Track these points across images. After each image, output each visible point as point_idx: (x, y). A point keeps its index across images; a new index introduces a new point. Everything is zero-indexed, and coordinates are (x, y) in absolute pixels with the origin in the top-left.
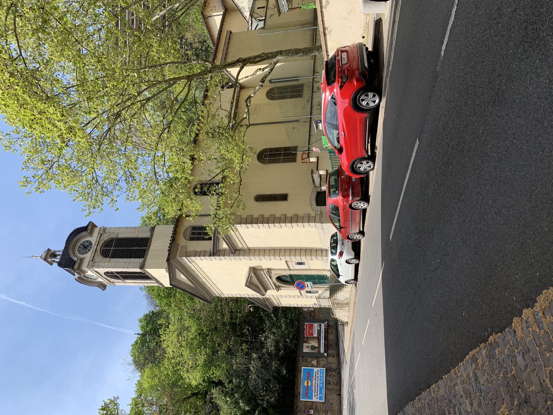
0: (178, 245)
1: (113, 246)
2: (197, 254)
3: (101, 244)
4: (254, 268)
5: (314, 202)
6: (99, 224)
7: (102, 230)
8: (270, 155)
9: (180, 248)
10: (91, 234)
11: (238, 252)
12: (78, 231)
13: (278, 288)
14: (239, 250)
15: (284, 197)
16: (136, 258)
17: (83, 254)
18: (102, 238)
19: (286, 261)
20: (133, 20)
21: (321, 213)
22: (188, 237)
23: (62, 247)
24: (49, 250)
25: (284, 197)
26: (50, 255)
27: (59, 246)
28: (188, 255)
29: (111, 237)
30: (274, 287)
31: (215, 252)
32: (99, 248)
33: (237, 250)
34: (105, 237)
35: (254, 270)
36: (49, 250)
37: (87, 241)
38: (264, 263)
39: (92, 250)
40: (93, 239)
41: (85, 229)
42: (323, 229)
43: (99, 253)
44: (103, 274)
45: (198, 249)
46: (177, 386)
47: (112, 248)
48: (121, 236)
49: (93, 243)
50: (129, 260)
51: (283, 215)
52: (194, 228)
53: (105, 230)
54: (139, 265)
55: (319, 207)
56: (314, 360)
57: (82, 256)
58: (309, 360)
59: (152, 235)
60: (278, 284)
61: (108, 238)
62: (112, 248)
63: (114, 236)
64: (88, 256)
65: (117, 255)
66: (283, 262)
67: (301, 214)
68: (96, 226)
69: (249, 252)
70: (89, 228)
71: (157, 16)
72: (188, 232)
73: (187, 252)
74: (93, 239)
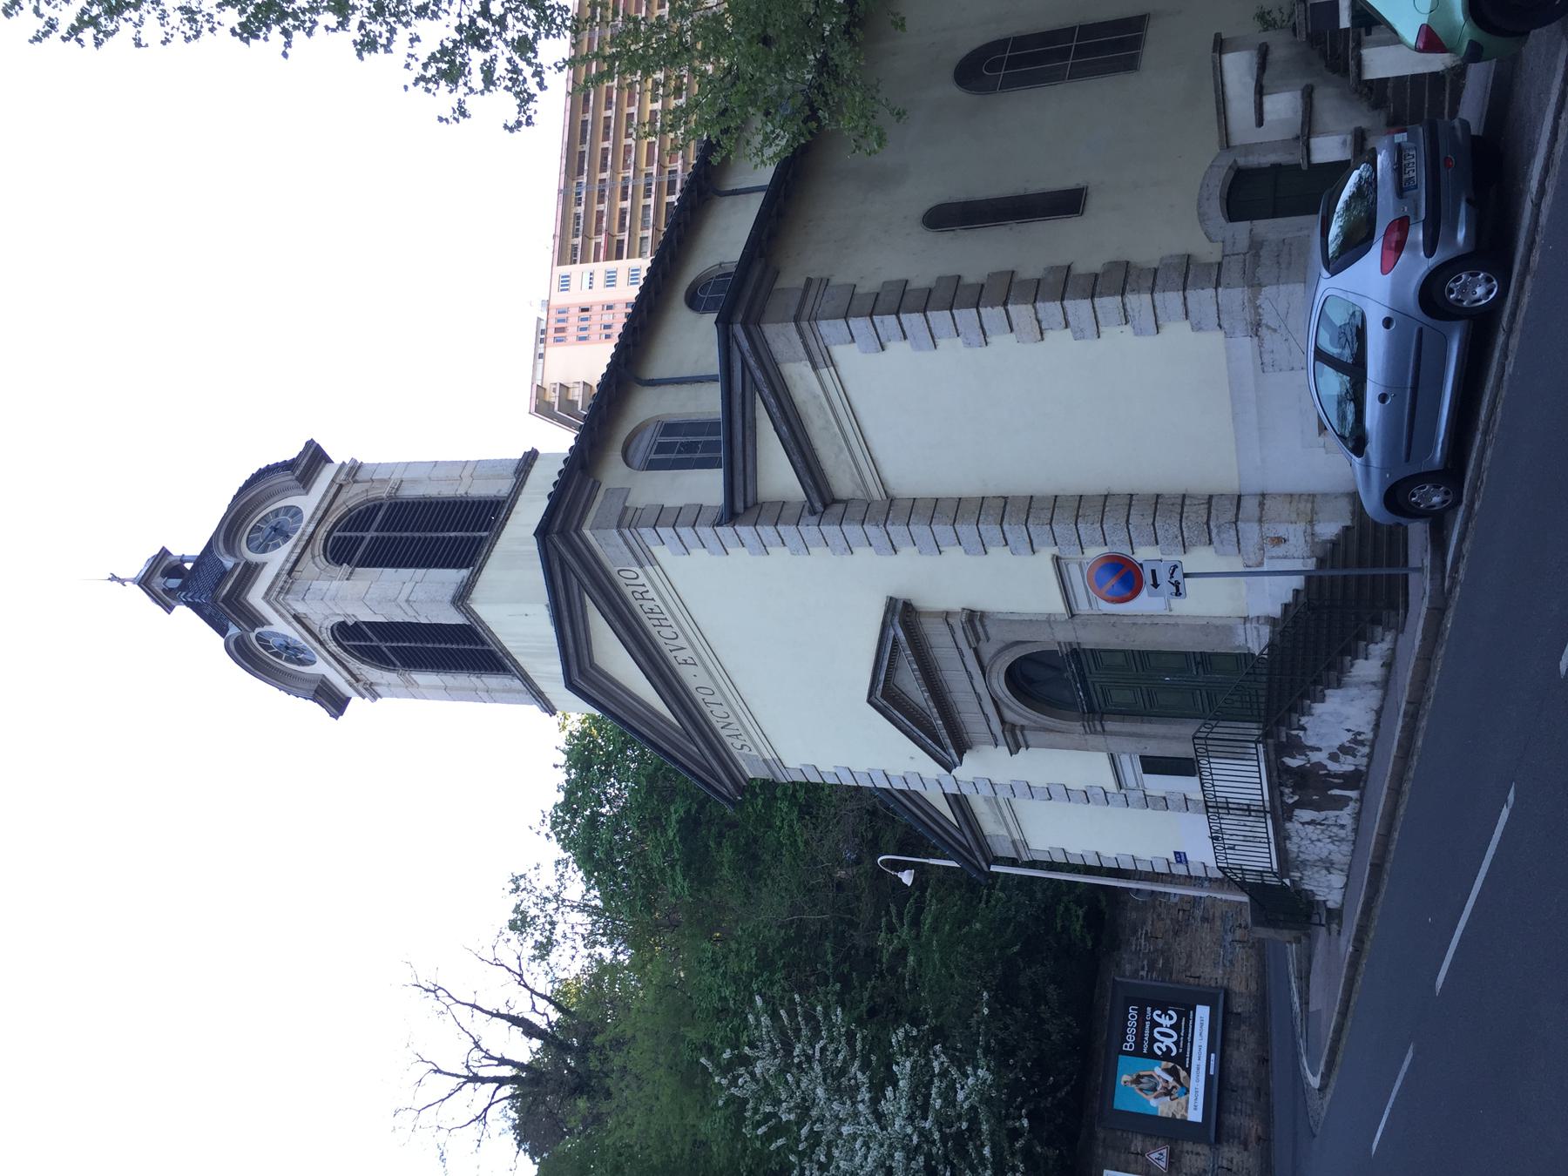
0: (597, 485)
1: (375, 525)
2: (664, 517)
3: (332, 519)
4: (908, 607)
5: (1215, 208)
6: (339, 453)
7: (346, 470)
8: (1013, 62)
9: (599, 498)
11: (839, 508)
13: (1015, 740)
14: (846, 502)
15: (1069, 203)
16: (448, 567)
17: (264, 551)
19: (1057, 560)
21: (1256, 246)
22: (638, 458)
24: (164, 553)
25: (1069, 203)
28: (627, 520)
29: (373, 494)
30: (996, 726)
31: (741, 507)
33: (835, 501)
34: (353, 496)
35: (902, 616)
36: (164, 553)
37: (288, 509)
38: (951, 578)
39: (295, 537)
40: (308, 503)
42: (1256, 328)
45: (673, 501)
47: (369, 535)
48: (410, 492)
49: (307, 514)
50: (420, 572)
51: (1052, 270)
52: (670, 428)
53: (353, 471)
54: (450, 591)
55: (1243, 227)
56: (1155, 1147)
57: (254, 557)
58: (1137, 1144)
60: (1018, 713)
62: (369, 535)
63: (383, 492)
64: (276, 559)
65: (385, 555)
66: (1043, 562)
67: (1146, 254)
68: (329, 461)
69: (888, 512)
72: (644, 444)
73: (626, 509)
74: (308, 503)
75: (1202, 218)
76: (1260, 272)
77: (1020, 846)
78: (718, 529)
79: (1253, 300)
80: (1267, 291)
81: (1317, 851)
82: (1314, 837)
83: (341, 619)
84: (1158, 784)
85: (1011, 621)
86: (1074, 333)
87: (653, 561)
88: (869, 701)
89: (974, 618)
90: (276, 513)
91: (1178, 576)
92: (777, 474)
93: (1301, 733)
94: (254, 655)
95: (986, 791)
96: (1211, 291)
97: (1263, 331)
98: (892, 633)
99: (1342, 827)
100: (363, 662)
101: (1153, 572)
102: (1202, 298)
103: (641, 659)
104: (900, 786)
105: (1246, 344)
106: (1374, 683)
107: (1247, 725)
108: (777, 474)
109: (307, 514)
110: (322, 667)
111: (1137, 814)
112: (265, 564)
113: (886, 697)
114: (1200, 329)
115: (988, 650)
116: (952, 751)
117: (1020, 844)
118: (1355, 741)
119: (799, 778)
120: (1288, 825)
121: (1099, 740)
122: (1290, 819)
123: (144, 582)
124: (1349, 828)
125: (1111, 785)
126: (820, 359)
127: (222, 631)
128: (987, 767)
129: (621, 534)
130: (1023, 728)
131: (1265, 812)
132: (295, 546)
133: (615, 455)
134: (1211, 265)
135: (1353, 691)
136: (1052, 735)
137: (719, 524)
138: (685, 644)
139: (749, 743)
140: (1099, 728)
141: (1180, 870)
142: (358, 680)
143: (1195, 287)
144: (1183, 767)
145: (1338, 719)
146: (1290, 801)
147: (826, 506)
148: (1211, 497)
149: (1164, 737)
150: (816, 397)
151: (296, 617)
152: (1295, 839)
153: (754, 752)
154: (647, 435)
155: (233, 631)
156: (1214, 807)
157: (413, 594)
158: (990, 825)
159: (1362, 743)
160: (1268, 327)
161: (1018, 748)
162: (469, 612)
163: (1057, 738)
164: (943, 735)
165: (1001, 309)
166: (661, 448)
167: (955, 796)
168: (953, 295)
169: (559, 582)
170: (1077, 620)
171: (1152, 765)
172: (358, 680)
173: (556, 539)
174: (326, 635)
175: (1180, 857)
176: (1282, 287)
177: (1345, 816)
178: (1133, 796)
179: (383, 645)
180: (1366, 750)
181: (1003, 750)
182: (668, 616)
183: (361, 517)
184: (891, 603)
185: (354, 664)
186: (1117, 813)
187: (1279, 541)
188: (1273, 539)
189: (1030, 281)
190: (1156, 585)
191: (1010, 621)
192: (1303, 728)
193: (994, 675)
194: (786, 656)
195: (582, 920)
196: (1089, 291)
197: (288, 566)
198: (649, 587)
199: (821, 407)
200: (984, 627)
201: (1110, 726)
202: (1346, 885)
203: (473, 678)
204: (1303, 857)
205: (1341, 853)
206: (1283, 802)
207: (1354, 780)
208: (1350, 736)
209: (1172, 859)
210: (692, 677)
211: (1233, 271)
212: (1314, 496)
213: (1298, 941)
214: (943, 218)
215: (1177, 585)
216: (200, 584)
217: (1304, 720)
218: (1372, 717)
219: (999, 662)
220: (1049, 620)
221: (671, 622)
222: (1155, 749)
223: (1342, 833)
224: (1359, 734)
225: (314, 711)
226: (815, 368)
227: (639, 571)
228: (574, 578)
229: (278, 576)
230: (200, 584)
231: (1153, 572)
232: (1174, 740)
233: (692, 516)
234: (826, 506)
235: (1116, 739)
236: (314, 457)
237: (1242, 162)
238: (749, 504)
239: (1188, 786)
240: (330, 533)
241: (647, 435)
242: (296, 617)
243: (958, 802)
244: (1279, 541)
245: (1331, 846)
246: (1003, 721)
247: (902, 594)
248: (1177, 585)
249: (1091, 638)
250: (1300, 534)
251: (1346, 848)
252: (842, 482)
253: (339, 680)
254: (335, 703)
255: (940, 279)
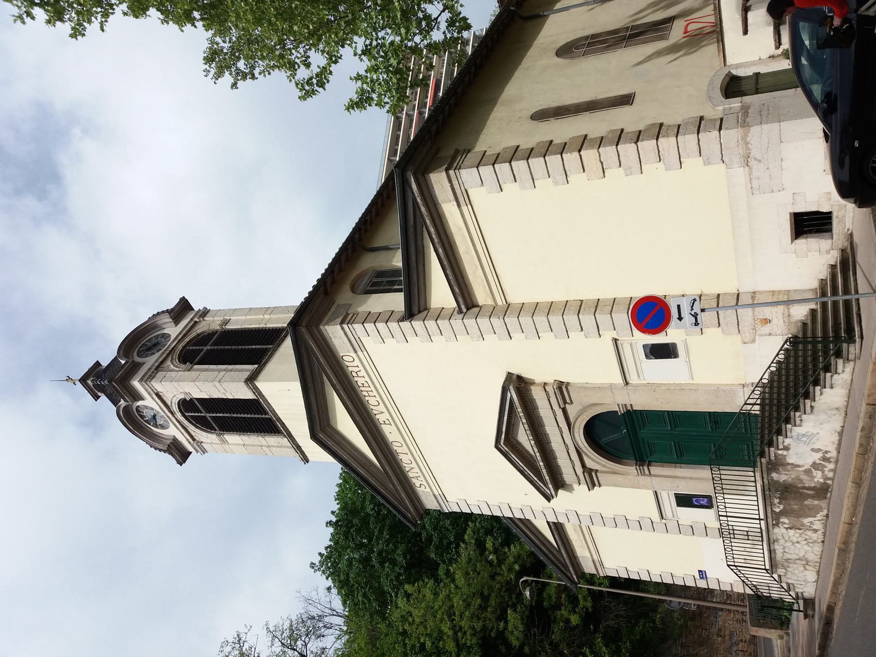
1: (210, 343)
3: (187, 340)
5: (718, 94)
6: (197, 306)
11: (476, 310)
13: (592, 479)
19: (615, 341)
21: (745, 109)
30: (579, 470)
31: (416, 307)
35: (518, 386)
42: (746, 160)
51: (612, 131)
57: (138, 359)
60: (594, 461)
62: (205, 348)
75: (711, 83)
76: (748, 120)
77: (598, 565)
78: (401, 323)
79: (744, 138)
80: (755, 130)
81: (797, 552)
82: (795, 540)
83: (182, 396)
84: (688, 515)
85: (586, 388)
86: (625, 170)
87: (363, 348)
88: (496, 447)
89: (562, 388)
90: (157, 337)
91: (697, 309)
92: (440, 292)
93: (785, 453)
94: (135, 421)
95: (573, 518)
96: (716, 133)
97: (752, 162)
98: (509, 394)
99: (816, 531)
100: (197, 427)
101: (679, 306)
102: (709, 137)
103: (345, 397)
104: (519, 515)
105: (740, 172)
106: (837, 409)
107: (746, 469)
108: (440, 292)
109: (173, 338)
110: (172, 431)
111: (674, 538)
112: (144, 363)
113: (507, 443)
114: (709, 163)
115: (572, 410)
116: (550, 486)
117: (598, 563)
118: (825, 459)
119: (456, 509)
120: (776, 530)
121: (647, 479)
122: (777, 525)
123: (83, 380)
124: (820, 532)
125: (656, 517)
126: (462, 198)
127: (115, 403)
128: (573, 505)
129: (343, 329)
130: (597, 471)
131: (760, 519)
132: (163, 353)
133: (347, 287)
134: (716, 120)
135: (822, 417)
136: (616, 476)
137: (402, 320)
138: (384, 410)
139: (424, 483)
140: (647, 472)
141: (702, 584)
142: (194, 440)
143: (705, 131)
144: (706, 502)
145: (814, 437)
146: (778, 510)
147: (468, 309)
148: (719, 295)
149: (691, 478)
150: (460, 229)
151: (158, 395)
152: (782, 541)
153: (428, 490)
154: (367, 277)
155: (122, 403)
156: (726, 533)
157: (226, 384)
158: (581, 551)
159: (827, 460)
160: (755, 159)
161: (594, 485)
162: (256, 390)
163: (619, 478)
164: (546, 475)
165: (576, 154)
166: (374, 284)
167: (554, 523)
168: (547, 149)
169: (306, 362)
170: (629, 387)
171: (684, 501)
172: (194, 440)
173: (304, 330)
174: (175, 408)
175: (702, 574)
176: (764, 126)
177: (817, 522)
178: (672, 525)
179: (208, 415)
180: (831, 466)
181: (584, 487)
182: (373, 388)
183: (204, 338)
184: (510, 375)
185: (191, 428)
186: (660, 537)
187: (766, 321)
188: (761, 320)
189: (596, 138)
190: (680, 318)
191: (586, 388)
192: (786, 448)
193: (576, 430)
194: (438, 404)
195: (339, 621)
196: (635, 139)
197: (157, 364)
198: (361, 368)
199: (464, 237)
200: (568, 392)
201: (655, 470)
202: (817, 581)
203: (260, 438)
204: (787, 556)
205: (813, 552)
206: (772, 511)
207: (822, 491)
208: (820, 455)
209: (697, 577)
210: (391, 433)
211: (729, 121)
212: (789, 291)
213: (781, 637)
214: (541, 116)
215: (695, 316)
216: (110, 381)
217: (787, 441)
218: (835, 438)
219: (579, 420)
220: (611, 387)
221: (375, 393)
222: (686, 489)
223: (815, 536)
224: (826, 452)
225: (169, 460)
226: (459, 205)
227: (354, 355)
228: (322, 374)
229: (149, 369)
230: (110, 381)
231: (679, 306)
232: (696, 479)
233: (388, 317)
234: (468, 309)
235: (658, 479)
236: (183, 307)
237: (734, 72)
238: (422, 309)
239: (706, 516)
240: (184, 347)
241: (367, 277)
242: (158, 395)
243: (557, 528)
244: (766, 321)
245: (806, 547)
246: (583, 465)
247: (516, 371)
248: (695, 316)
249: (642, 402)
250: (780, 316)
251: (818, 548)
252: (481, 296)
253: (183, 439)
254: (181, 454)
255: (538, 144)
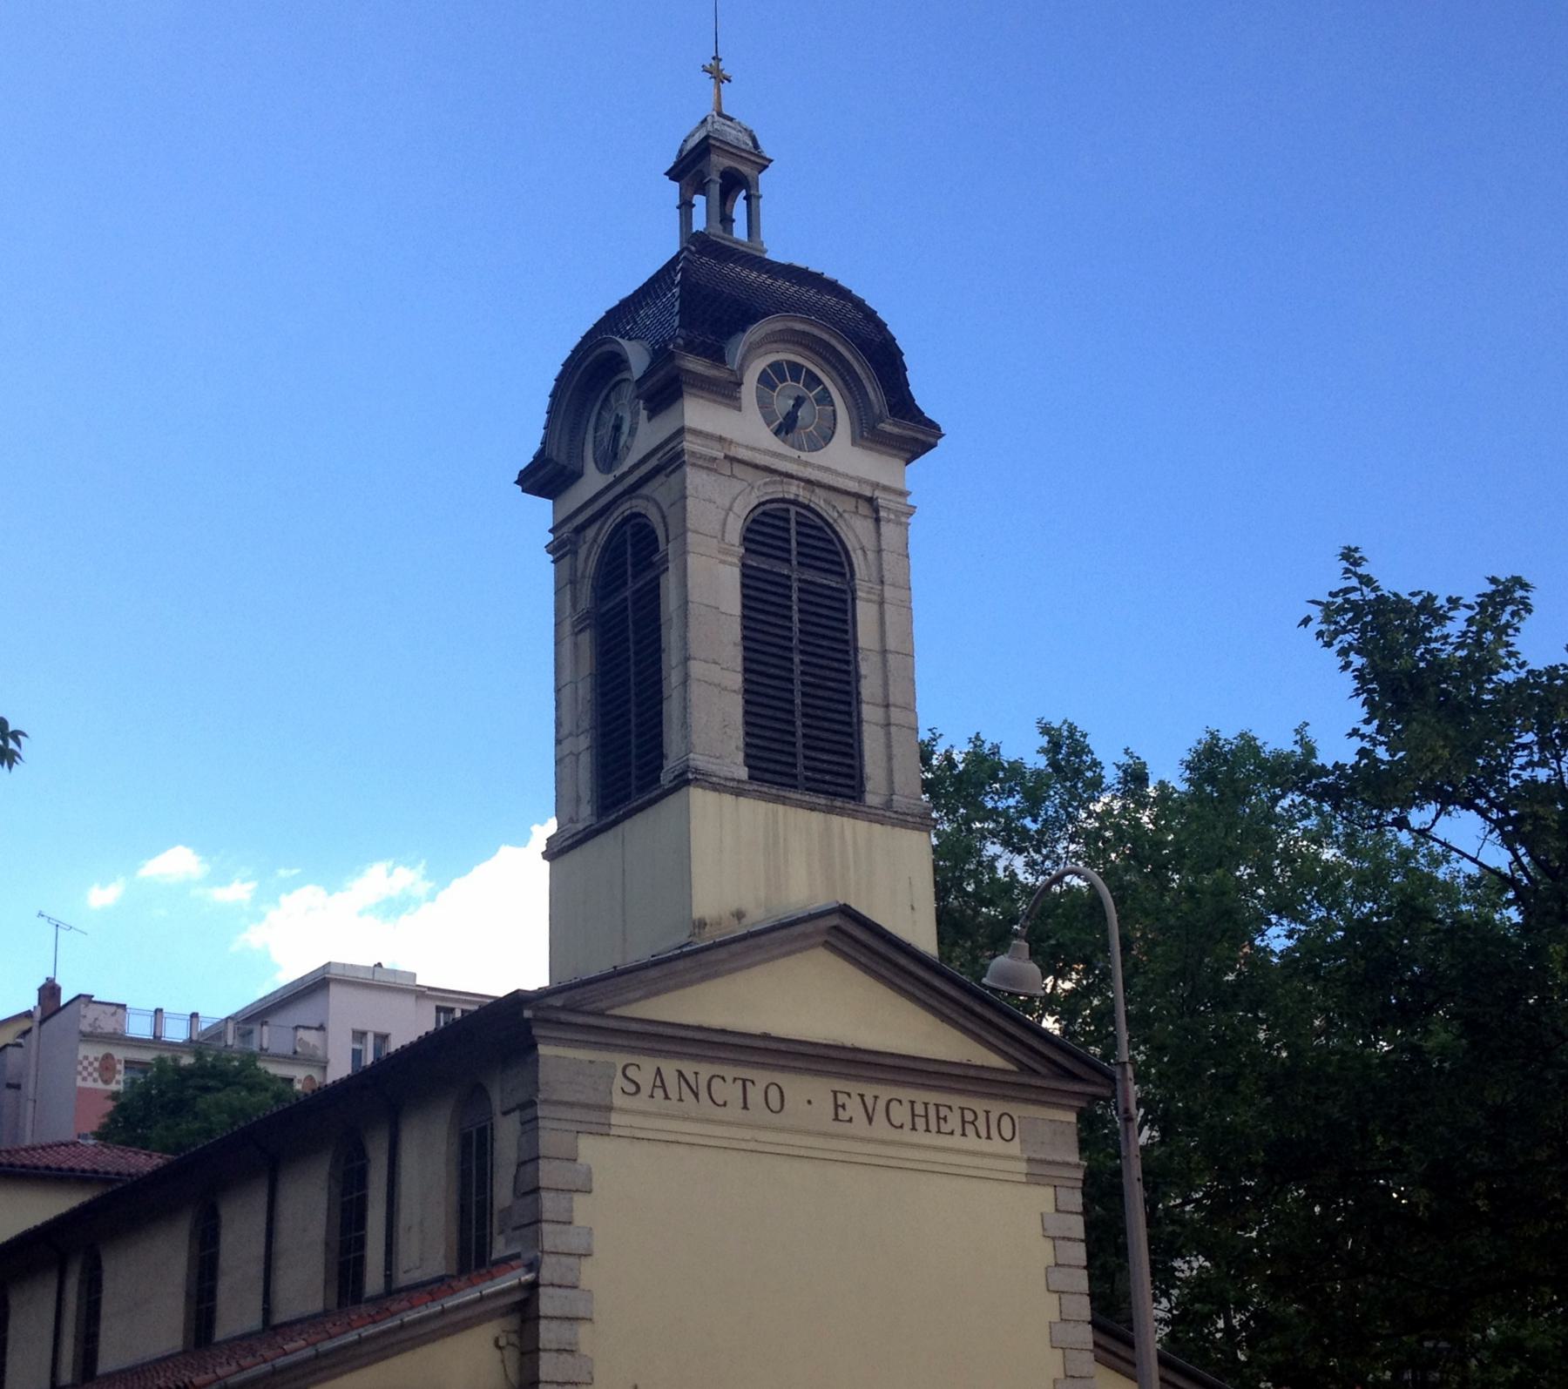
1: (809, 575)
3: (819, 501)
10: (869, 435)
12: (885, 358)
18: (847, 504)
20: (807, 778)
23: (777, 250)
24: (763, 164)
26: (714, 168)
27: (791, 226)
29: (857, 559)
32: (793, 490)
34: (855, 531)
41: (902, 404)
43: (777, 491)
44: (637, 505)
46: (1184, 856)
59: (875, 817)
61: (851, 543)
70: (907, 431)
71: (1124, 1054)
